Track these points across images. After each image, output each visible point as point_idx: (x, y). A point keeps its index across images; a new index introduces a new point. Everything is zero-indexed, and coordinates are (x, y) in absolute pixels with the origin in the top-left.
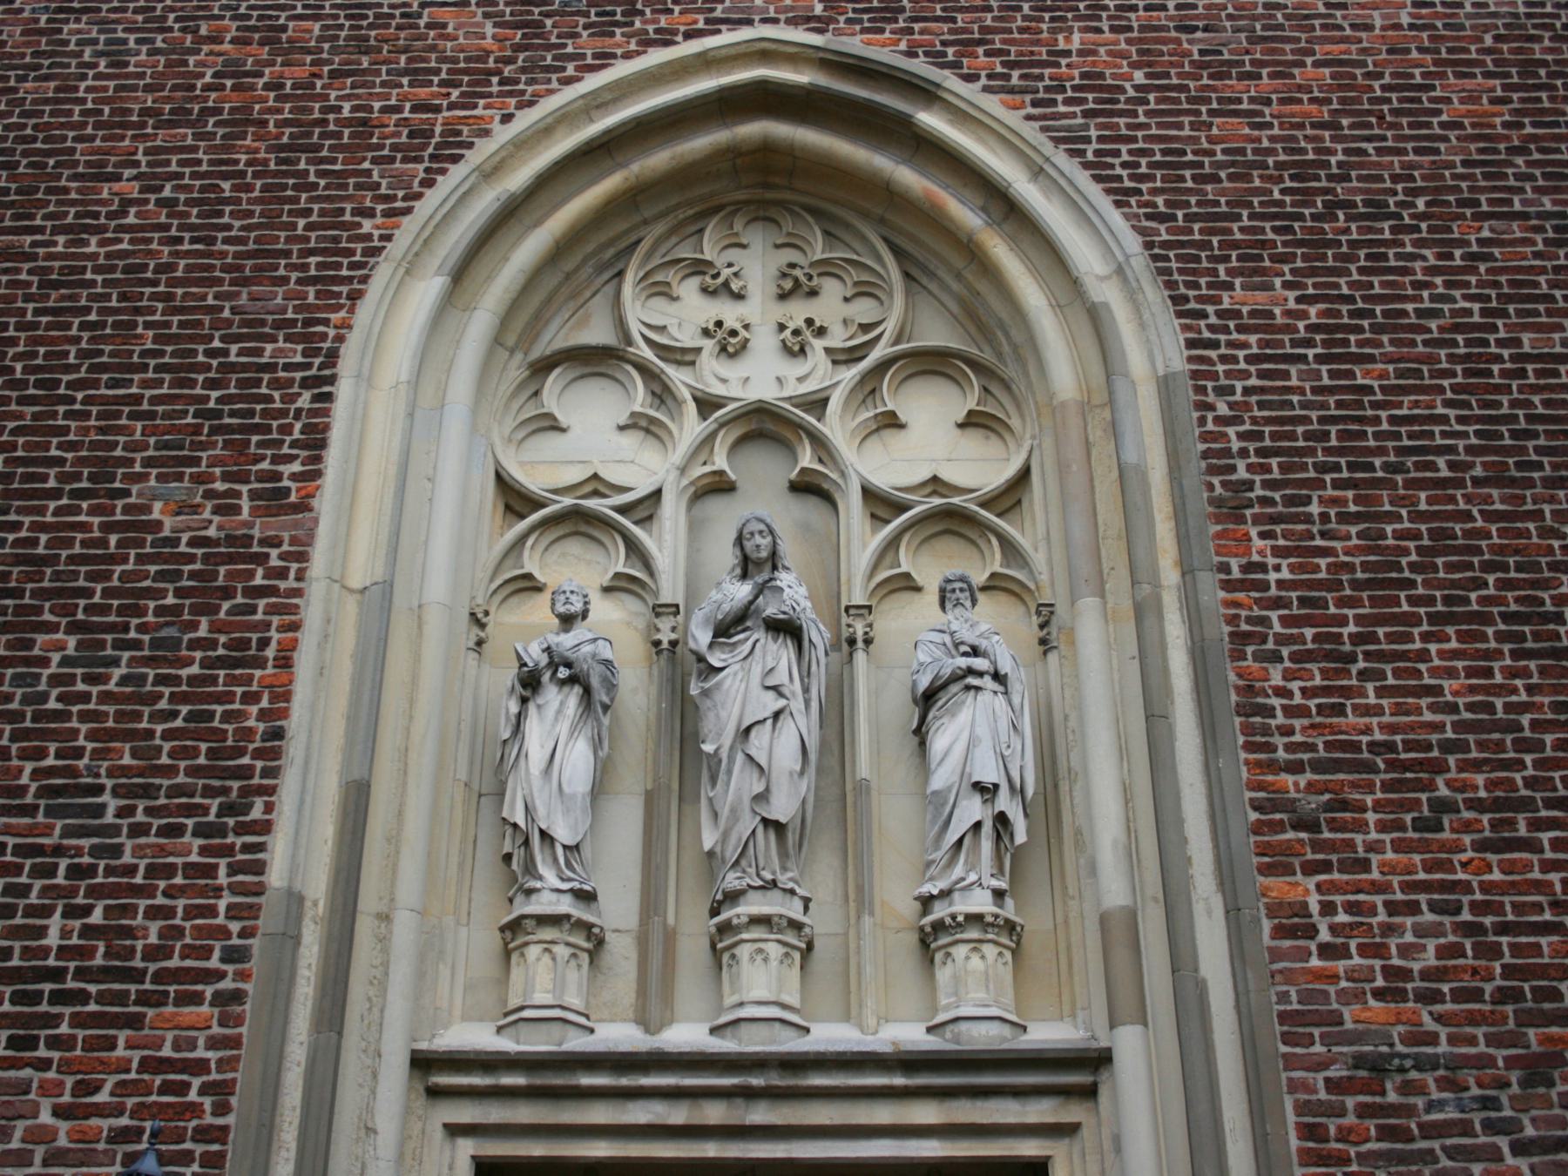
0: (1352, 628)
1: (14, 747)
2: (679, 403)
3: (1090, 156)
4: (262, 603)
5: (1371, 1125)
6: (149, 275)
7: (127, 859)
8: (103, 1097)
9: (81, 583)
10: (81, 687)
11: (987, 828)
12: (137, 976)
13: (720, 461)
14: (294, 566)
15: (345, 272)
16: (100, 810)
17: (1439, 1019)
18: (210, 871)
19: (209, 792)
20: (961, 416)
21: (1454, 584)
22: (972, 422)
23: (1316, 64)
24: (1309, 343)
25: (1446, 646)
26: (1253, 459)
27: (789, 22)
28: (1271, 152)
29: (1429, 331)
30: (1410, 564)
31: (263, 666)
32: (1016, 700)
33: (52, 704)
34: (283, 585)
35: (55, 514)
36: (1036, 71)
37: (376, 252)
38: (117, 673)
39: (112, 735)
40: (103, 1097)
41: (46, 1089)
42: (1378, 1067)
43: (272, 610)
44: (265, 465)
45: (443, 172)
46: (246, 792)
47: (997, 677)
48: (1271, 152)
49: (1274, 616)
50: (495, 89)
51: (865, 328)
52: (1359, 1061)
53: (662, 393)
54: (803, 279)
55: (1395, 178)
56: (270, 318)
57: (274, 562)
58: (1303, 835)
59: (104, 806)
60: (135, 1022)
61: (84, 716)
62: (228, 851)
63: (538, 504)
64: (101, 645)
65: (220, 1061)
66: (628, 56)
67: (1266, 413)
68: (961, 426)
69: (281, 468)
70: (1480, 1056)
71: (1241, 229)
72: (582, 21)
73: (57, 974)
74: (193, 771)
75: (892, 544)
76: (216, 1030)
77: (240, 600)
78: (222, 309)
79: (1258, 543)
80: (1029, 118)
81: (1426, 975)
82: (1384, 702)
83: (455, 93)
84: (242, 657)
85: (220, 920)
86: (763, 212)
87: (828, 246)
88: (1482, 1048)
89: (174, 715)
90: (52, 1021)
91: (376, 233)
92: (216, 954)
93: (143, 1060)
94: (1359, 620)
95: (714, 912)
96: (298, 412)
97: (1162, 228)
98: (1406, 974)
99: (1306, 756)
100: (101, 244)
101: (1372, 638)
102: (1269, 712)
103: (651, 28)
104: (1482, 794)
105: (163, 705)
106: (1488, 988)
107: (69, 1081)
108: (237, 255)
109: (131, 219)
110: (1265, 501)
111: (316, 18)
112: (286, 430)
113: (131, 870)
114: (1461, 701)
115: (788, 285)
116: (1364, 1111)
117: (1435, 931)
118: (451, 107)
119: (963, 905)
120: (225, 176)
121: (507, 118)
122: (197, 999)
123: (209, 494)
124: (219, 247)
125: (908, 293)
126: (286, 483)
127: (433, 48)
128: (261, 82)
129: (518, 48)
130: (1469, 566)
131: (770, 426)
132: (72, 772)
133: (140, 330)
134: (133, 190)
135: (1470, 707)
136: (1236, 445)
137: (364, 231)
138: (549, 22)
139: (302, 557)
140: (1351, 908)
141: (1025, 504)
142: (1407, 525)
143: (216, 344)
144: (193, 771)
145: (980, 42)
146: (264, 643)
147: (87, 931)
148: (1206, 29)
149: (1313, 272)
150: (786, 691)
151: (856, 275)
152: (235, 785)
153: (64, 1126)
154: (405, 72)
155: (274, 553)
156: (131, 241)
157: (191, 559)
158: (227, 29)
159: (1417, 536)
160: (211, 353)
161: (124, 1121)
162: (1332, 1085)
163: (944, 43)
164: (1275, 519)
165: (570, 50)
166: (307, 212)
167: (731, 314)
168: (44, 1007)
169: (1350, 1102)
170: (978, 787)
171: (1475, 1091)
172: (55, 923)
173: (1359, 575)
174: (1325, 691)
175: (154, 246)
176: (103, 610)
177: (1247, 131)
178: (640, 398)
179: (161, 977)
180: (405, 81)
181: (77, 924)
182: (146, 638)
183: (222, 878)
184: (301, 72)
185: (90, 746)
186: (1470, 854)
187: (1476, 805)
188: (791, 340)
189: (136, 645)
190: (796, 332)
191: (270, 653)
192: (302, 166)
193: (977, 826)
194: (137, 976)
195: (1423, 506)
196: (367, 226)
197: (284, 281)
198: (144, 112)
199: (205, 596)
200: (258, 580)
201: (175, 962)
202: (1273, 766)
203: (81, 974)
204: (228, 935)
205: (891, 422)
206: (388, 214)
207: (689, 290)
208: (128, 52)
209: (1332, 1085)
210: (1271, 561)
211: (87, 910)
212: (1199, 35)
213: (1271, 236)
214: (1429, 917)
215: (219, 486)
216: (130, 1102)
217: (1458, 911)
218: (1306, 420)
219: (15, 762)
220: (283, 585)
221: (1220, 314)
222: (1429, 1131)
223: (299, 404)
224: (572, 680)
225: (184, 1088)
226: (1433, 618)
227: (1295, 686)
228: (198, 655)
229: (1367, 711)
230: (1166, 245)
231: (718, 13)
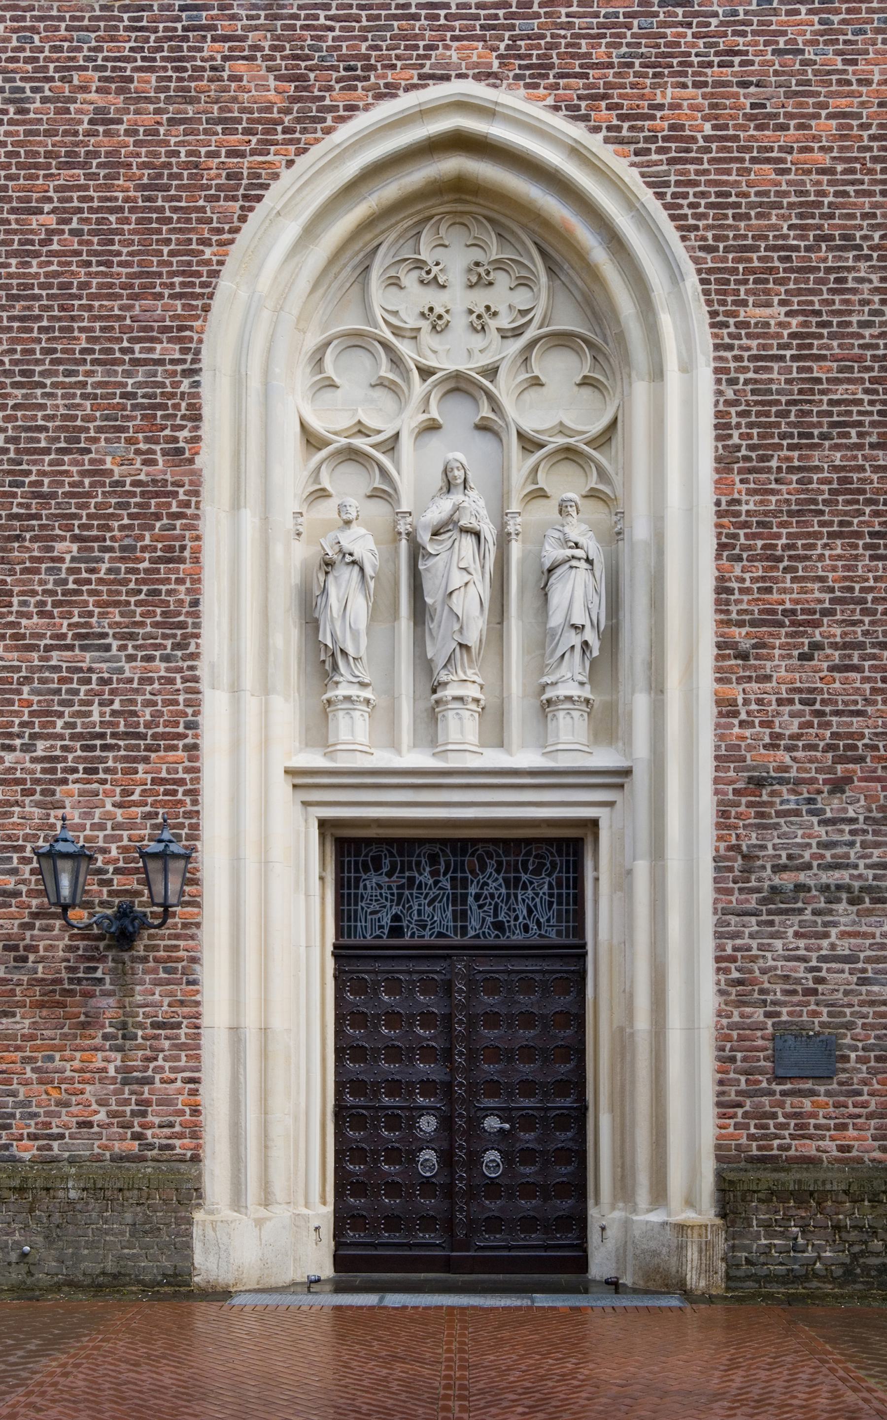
0: (784, 541)
1: (55, 611)
2: (408, 371)
3: (668, 199)
4: (178, 523)
5: (752, 811)
6: (74, 291)
7: (127, 674)
8: (135, 797)
9: (73, 510)
10: (85, 575)
11: (578, 650)
12: (143, 737)
13: (434, 413)
14: (194, 499)
15: (198, 290)
16: (108, 648)
17: (794, 759)
18: (172, 681)
19: (165, 637)
20: (578, 379)
21: (846, 513)
22: (586, 382)
23: (830, 116)
24: (787, 346)
25: (834, 552)
26: (744, 430)
27: (477, 77)
28: (786, 194)
29: (863, 337)
30: (824, 501)
31: (184, 562)
32: (597, 574)
33: (71, 586)
34: (189, 512)
35: (50, 465)
36: (640, 123)
37: (215, 274)
38: (104, 567)
39: (108, 604)
40: (135, 797)
41: (106, 794)
42: (759, 783)
43: (185, 527)
44: (167, 432)
45: (251, 209)
46: (185, 637)
47: (589, 561)
48: (786, 194)
49: (741, 532)
50: (280, 137)
51: (523, 313)
52: (750, 780)
53: (396, 361)
54: (483, 274)
55: (865, 216)
56: (156, 324)
57: (182, 497)
58: (740, 662)
59: (110, 645)
60: (146, 760)
61: (91, 593)
62: (180, 670)
63: (327, 443)
64: (92, 549)
65: (191, 779)
66: (367, 108)
67: (755, 398)
68: (579, 385)
69: (177, 434)
70: (811, 779)
71: (760, 259)
72: (335, 75)
73: (102, 736)
74: (156, 625)
75: (535, 470)
76: (187, 764)
77: (165, 521)
78: (125, 318)
79: (738, 486)
80: (633, 165)
81: (791, 737)
82: (795, 586)
83: (254, 140)
84: (172, 556)
85: (181, 707)
86: (459, 220)
87: (501, 250)
88: (813, 774)
89: (140, 592)
90: (104, 760)
91: (214, 259)
92: (182, 725)
93: (153, 779)
94: (789, 536)
95: (434, 691)
96: (183, 393)
97: (709, 257)
98: (779, 736)
99: (747, 617)
100: (41, 265)
101: (792, 547)
102: (730, 591)
103: (382, 82)
104: (838, 639)
105: (132, 585)
106: (822, 744)
107: (118, 790)
108: (129, 276)
109: (55, 247)
110: (747, 459)
111: (152, 69)
112: (176, 407)
113: (130, 681)
114: (837, 585)
115: (474, 279)
116: (750, 805)
117: (800, 714)
118: (253, 153)
119: (562, 691)
120: (111, 211)
121: (290, 163)
122: (174, 748)
123: (138, 452)
124: (116, 269)
125: (550, 278)
126: (181, 444)
127: (235, 99)
128: (122, 128)
129: (294, 100)
130: (857, 502)
131: (463, 385)
132: (87, 625)
133: (76, 334)
134: (51, 221)
135: (842, 589)
136: (734, 420)
137: (206, 257)
138: (312, 75)
139: (197, 493)
140: (759, 702)
141: (613, 442)
142: (826, 475)
143: (125, 344)
144: (156, 625)
145: (605, 97)
146: (183, 548)
147: (114, 713)
148: (757, 86)
149: (799, 292)
150: (471, 570)
151: (516, 271)
152: (179, 632)
153: (119, 811)
154: (220, 121)
155: (181, 491)
156: (60, 264)
157: (133, 494)
158: (91, 80)
159: (829, 482)
160: (123, 351)
161: (148, 809)
162: (736, 792)
163: (579, 98)
164: (750, 471)
165: (327, 102)
166: (168, 242)
167: (438, 300)
168: (98, 753)
169: (744, 800)
170: (574, 627)
171: (806, 795)
172: (95, 709)
173: (793, 507)
174: (763, 579)
175: (74, 268)
176: (89, 527)
177: (773, 176)
178: (385, 371)
179: (155, 736)
180: (219, 128)
181: (107, 709)
182: (116, 545)
183: (179, 685)
184: (149, 119)
185: (97, 610)
186: (825, 673)
187: (835, 646)
188: (477, 324)
189: (111, 549)
190: (479, 317)
191: (187, 554)
192: (160, 203)
193: (573, 647)
194: (143, 737)
195: (837, 463)
196: (208, 252)
197: (160, 296)
198: (48, 154)
199: (146, 519)
200: (174, 509)
201: (160, 730)
202: (728, 623)
203: (114, 735)
204: (186, 715)
205: (536, 382)
206: (221, 244)
207: (410, 279)
208: (27, 100)
209: (736, 792)
210: (744, 498)
211: (112, 702)
212: (752, 89)
213: (777, 264)
214: (798, 707)
215: (142, 446)
216: (150, 800)
217: (814, 704)
218: (777, 402)
219: (57, 620)
220: (189, 512)
221: (738, 325)
222: (779, 814)
223: (182, 389)
224: (354, 562)
225: (174, 793)
226: (831, 535)
227: (747, 576)
228: (147, 555)
229: (784, 591)
230: (710, 271)
231: (426, 70)
